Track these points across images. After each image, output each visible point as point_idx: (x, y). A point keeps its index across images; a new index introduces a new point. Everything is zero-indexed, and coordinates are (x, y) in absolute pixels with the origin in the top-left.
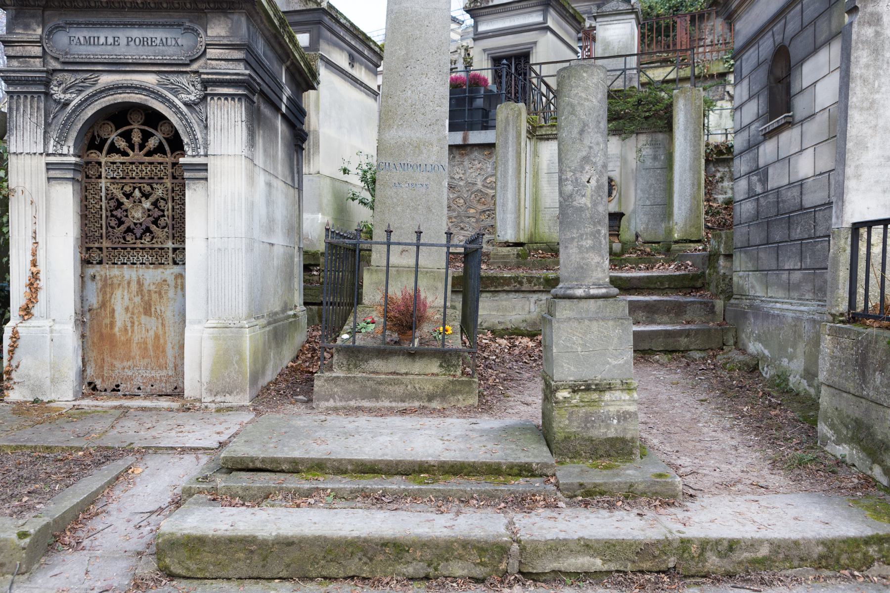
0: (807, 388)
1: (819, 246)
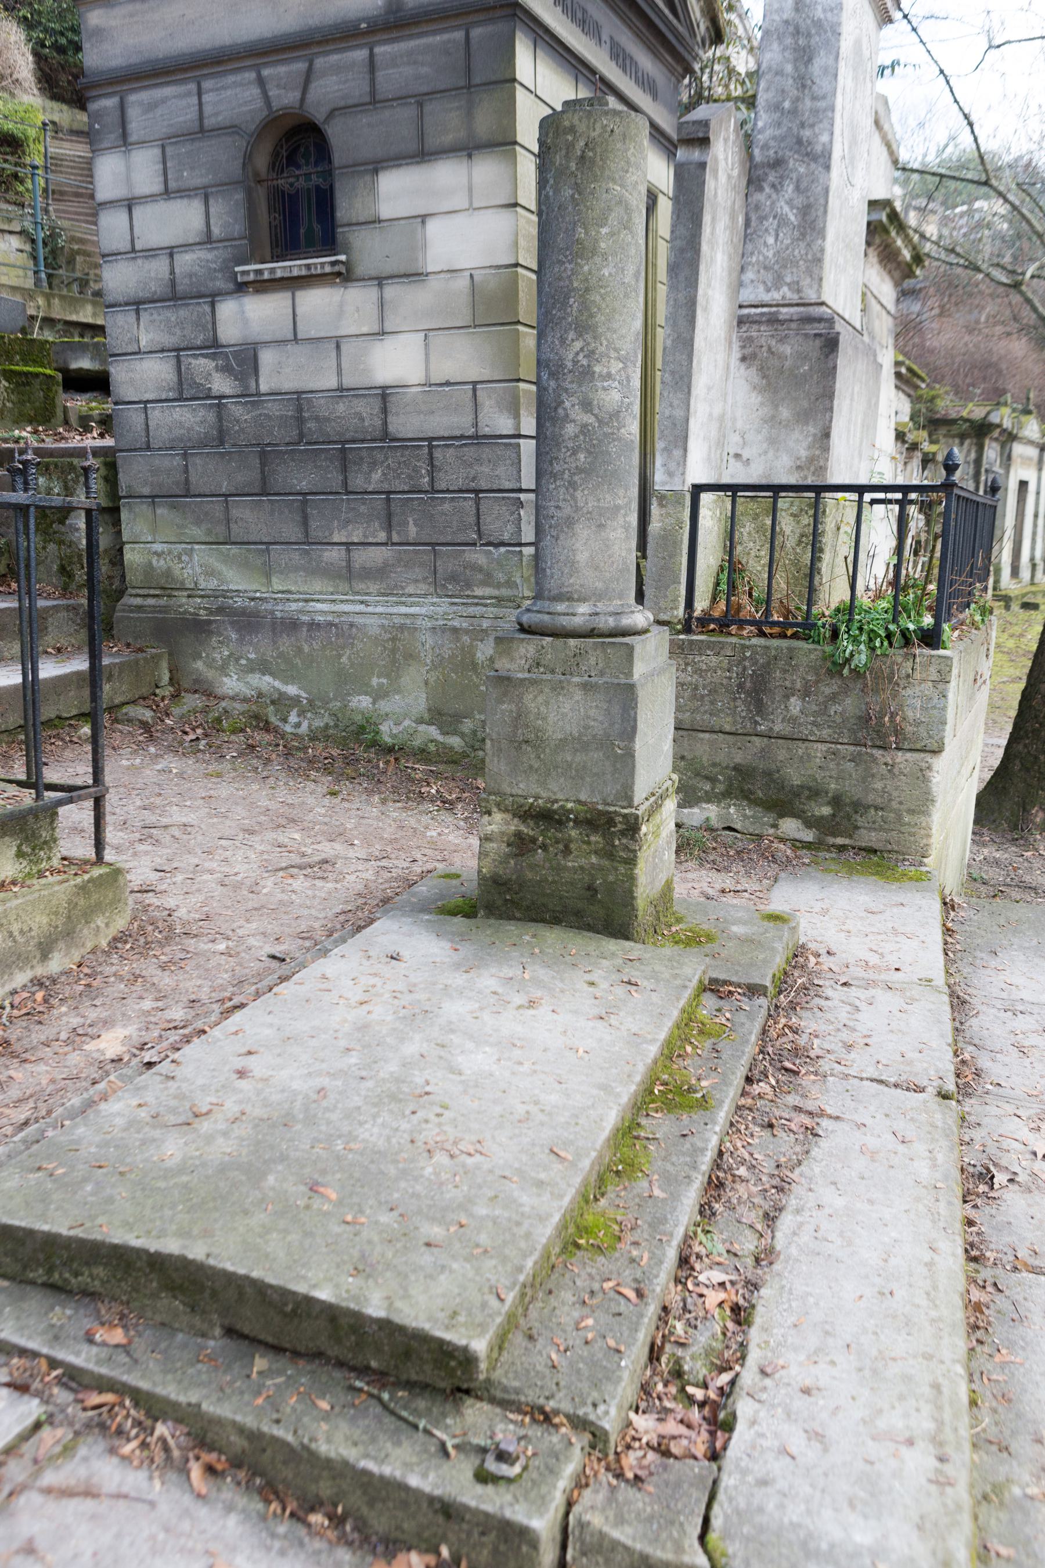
0: (440, 738)
1: (447, 506)
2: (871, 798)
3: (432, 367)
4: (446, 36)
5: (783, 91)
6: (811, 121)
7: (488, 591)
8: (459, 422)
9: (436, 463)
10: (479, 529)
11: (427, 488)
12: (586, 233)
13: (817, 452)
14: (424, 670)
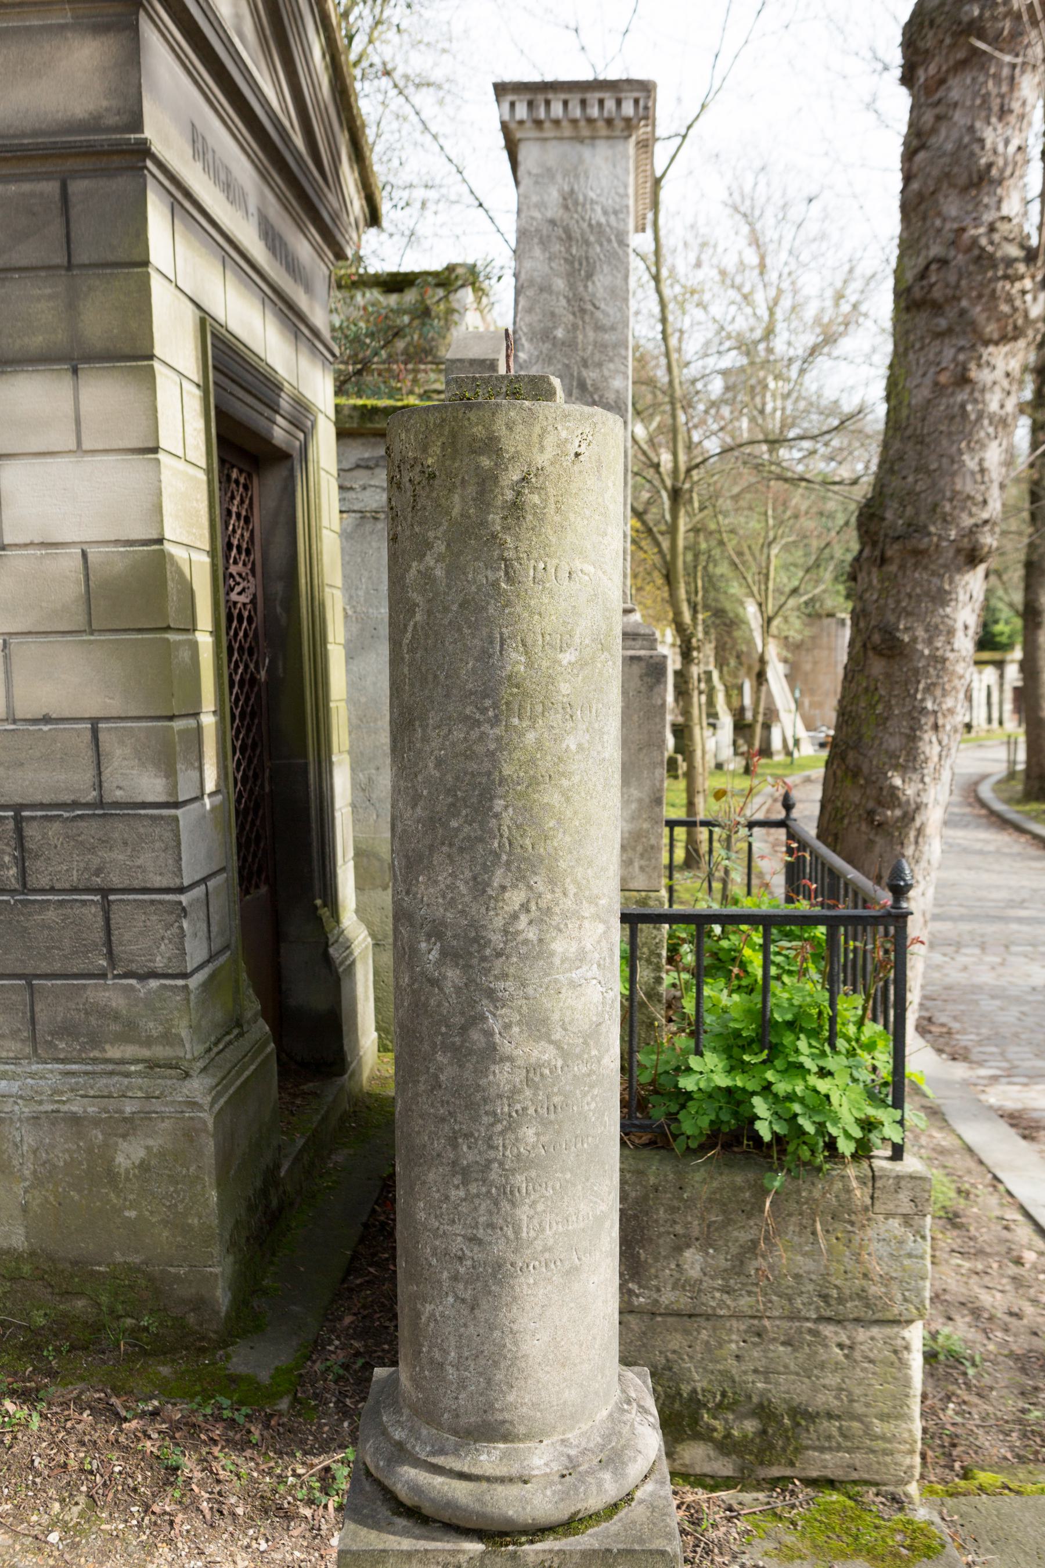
1: (51, 915)
2: (825, 1400)
3: (18, 692)
4: (26, 187)
5: (553, 314)
6: (597, 358)
7: (130, 1051)
8: (74, 781)
9: (29, 845)
10: (110, 952)
11: (15, 884)
12: (530, 665)
13: (646, 826)
14: (19, 1189)
